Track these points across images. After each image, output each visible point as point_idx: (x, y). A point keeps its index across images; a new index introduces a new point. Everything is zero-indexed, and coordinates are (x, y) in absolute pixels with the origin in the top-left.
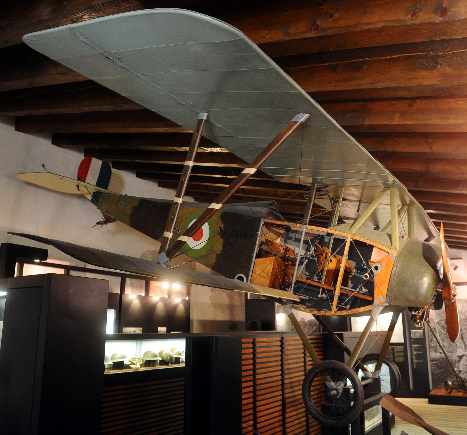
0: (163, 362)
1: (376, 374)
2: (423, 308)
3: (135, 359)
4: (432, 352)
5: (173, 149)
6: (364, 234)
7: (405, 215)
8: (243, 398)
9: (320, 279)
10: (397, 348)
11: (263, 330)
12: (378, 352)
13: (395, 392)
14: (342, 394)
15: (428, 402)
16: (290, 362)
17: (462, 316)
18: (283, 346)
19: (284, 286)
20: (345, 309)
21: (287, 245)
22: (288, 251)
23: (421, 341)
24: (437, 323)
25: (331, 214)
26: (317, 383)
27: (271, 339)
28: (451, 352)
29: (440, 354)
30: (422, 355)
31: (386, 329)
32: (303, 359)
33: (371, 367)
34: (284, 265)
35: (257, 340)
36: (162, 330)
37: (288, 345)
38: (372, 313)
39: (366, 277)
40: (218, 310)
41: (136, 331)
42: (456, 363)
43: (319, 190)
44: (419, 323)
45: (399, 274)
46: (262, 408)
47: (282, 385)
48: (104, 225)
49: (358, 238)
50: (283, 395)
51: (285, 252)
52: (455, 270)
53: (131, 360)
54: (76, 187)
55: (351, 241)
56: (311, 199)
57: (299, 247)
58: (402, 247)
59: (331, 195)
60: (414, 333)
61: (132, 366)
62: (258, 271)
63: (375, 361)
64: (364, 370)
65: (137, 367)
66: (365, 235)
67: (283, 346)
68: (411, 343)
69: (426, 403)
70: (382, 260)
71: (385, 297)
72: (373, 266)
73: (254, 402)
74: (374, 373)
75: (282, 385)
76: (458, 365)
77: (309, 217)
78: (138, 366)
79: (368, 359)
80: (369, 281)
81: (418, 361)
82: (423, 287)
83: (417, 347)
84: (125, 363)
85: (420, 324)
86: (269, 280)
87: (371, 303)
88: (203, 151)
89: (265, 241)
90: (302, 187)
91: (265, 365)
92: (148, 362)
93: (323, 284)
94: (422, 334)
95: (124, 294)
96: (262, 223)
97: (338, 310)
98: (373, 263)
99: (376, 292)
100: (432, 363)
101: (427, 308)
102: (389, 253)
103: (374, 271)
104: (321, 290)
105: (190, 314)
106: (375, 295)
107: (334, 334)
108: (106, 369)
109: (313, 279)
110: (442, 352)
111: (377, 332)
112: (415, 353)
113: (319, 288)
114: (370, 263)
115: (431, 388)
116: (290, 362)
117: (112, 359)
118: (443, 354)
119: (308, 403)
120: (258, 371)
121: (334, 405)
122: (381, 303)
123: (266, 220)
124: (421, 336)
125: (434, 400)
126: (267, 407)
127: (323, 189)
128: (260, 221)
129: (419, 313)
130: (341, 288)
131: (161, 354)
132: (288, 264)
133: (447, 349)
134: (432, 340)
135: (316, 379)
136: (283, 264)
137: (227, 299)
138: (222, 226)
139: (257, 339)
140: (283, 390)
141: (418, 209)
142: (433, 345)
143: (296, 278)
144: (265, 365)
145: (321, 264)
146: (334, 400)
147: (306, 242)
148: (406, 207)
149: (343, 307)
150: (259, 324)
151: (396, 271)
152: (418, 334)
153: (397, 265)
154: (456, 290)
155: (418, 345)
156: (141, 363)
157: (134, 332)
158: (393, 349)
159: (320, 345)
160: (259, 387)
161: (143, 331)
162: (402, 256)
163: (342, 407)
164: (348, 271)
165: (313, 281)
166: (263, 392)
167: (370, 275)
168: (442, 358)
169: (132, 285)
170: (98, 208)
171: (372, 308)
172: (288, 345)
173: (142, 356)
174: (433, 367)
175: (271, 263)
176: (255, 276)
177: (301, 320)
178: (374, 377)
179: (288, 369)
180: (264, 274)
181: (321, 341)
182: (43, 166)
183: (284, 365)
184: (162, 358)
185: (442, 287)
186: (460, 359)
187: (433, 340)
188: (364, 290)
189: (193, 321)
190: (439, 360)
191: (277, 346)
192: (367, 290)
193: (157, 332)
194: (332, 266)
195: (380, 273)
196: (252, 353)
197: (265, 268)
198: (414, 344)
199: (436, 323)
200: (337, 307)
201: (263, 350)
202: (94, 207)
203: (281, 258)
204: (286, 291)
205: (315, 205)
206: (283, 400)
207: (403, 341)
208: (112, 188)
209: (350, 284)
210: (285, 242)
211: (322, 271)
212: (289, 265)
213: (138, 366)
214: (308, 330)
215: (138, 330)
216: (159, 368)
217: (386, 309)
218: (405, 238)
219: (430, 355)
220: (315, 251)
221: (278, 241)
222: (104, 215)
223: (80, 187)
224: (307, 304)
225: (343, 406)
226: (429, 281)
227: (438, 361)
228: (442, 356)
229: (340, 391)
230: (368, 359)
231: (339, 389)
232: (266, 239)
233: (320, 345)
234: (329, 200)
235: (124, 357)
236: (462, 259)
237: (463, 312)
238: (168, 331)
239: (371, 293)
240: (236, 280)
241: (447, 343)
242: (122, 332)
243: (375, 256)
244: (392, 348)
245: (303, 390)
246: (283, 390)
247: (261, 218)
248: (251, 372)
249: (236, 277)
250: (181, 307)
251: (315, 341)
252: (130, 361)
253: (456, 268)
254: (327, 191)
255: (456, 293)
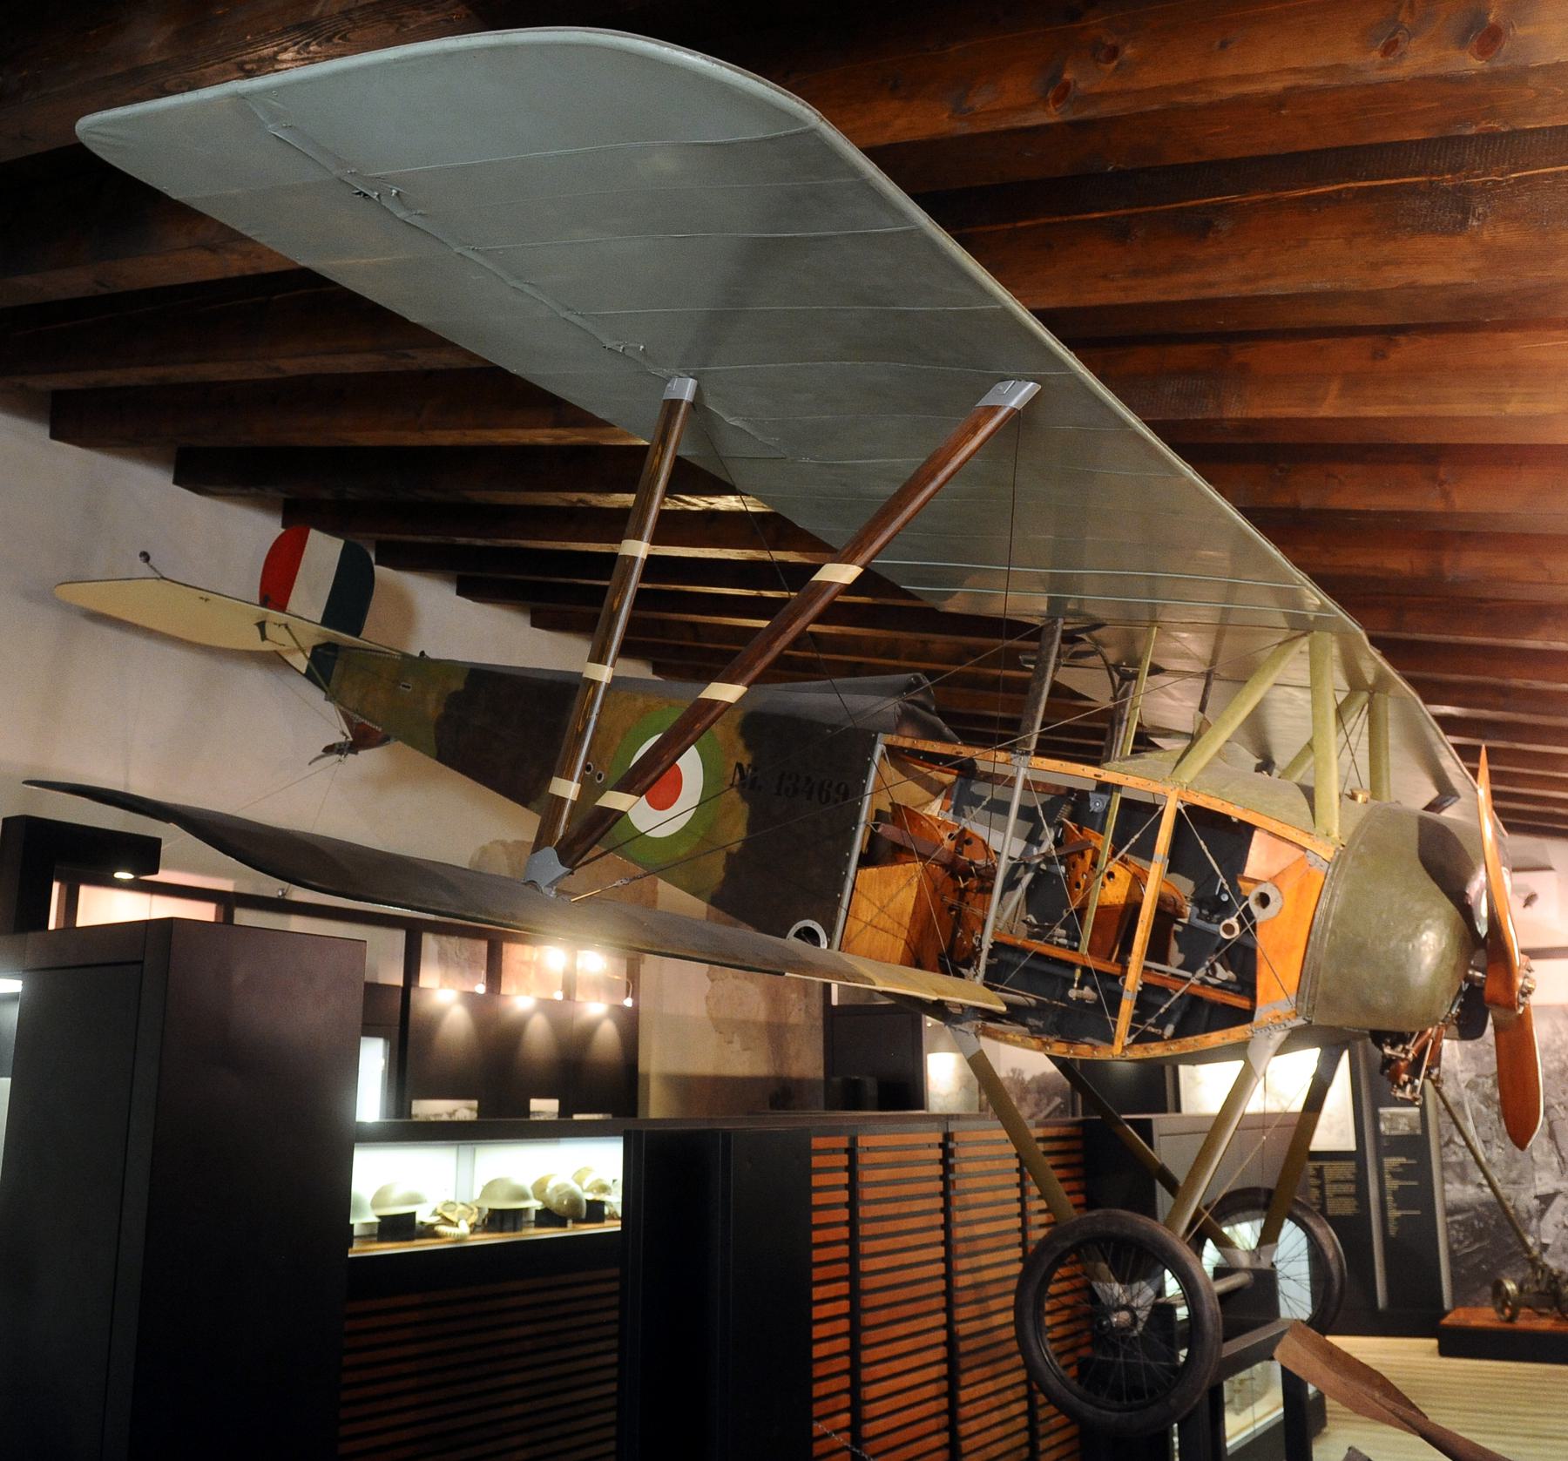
0: (547, 1217)
1: (1262, 1257)
2: (1422, 1033)
3: (452, 1207)
4: (1451, 1183)
5: (580, 501)
6: (1224, 787)
7: (1358, 723)
8: (815, 1336)
9: (1074, 937)
10: (1332, 1170)
11: (882, 1107)
12: (1270, 1182)
13: (1327, 1317)
14: (1148, 1323)
15: (1437, 1350)
16: (974, 1214)
17: (1551, 1062)
18: (951, 1161)
19: (954, 961)
20: (1158, 1038)
21: (964, 823)
22: (968, 842)
23: (1415, 1145)
24: (1467, 1087)
25: (1112, 718)
26: (1064, 1286)
27: (910, 1139)
28: (1514, 1183)
29: (1478, 1190)
30: (1418, 1194)
31: (1297, 1105)
32: (1019, 1205)
33: (1245, 1234)
34: (955, 891)
35: (864, 1141)
36: (545, 1107)
37: (969, 1159)
38: (1251, 1053)
39: (1229, 929)
40: (730, 1042)
41: (455, 1111)
42: (1530, 1218)
43: (1070, 638)
44: (1405, 1084)
45: (1341, 920)
46: (881, 1370)
47: (948, 1293)
48: (351, 756)
49: (1201, 801)
50: (949, 1326)
51: (957, 845)
52: (1528, 908)
53: (439, 1211)
54: (257, 630)
55: (1179, 811)
56: (1045, 670)
57: (1003, 829)
58: (1350, 830)
59: (1112, 655)
60: (1391, 1120)
61: (442, 1229)
62: (866, 911)
63: (1258, 1213)
64: (1223, 1243)
65: (462, 1231)
66: (1226, 790)
67: (951, 1161)
68: (1380, 1154)
69: (1431, 1353)
70: (1282, 873)
71: (1293, 998)
72: (1253, 894)
73: (854, 1352)
74: (1254, 1254)
75: (948, 1293)
76: (1538, 1226)
77: (1037, 729)
78: (464, 1229)
79: (1235, 1204)
80: (1238, 944)
81: (1405, 1213)
82: (1419, 964)
83: (1402, 1165)
84: (419, 1218)
85: (1409, 1087)
86: (903, 942)
87: (1246, 1016)
88: (680, 506)
89: (889, 809)
90: (1014, 628)
91: (889, 1226)
92: (498, 1217)
93: (1083, 955)
94: (1417, 1123)
95: (418, 986)
96: (880, 748)
97: (1135, 1042)
98: (1252, 885)
99: (1262, 980)
100: (1449, 1219)
101: (1434, 1035)
102: (1305, 849)
103: (1256, 909)
104: (1078, 973)
105: (637, 1055)
106: (1260, 992)
107: (1120, 1123)
108: (355, 1240)
109: (1052, 936)
110: (1484, 1182)
111: (1264, 1116)
112: (1392, 1184)
113: (1072, 966)
114: (1241, 883)
115: (1447, 1304)
116: (974, 1214)
117: (374, 1205)
118: (1488, 1190)
119: (1036, 1353)
120: (867, 1247)
121: (1121, 1359)
122: (1278, 1017)
123: (895, 737)
124: (1412, 1128)
125: (1457, 1343)
126: (897, 1366)
127: (1083, 636)
128: (874, 742)
129: (1407, 1052)
130: (1145, 968)
131: (539, 1189)
132: (966, 887)
133: (1501, 1171)
134: (1451, 1141)
135: (1062, 1272)
136: (951, 888)
137: (763, 1005)
138: (746, 760)
139: (864, 1138)
140: (949, 1309)
141: (1402, 700)
142: (1453, 1159)
143: (994, 934)
144: (889, 1226)
145: (1078, 885)
146: (1120, 1344)
147: (1026, 813)
148: (1364, 696)
149: (1153, 1030)
150: (871, 1087)
151: (1329, 909)
152: (1403, 1121)
153: (1334, 889)
154: (1532, 975)
155: (1403, 1160)
156: (474, 1219)
157: (452, 1114)
158: (1319, 1173)
159: (1074, 1159)
160: (869, 1301)
161: (481, 1111)
162: (1350, 858)
163: (1147, 1367)
164: (1169, 909)
165: (1052, 943)
166: (883, 1315)
167: (1242, 925)
168: (1484, 1204)
169: (443, 958)
170: (330, 697)
171: (1250, 1034)
172: (969, 1159)
173: (477, 1195)
174: (1454, 1232)
175: (909, 884)
176: (856, 927)
177: (1011, 1074)
178: (1257, 1266)
179: (966, 1240)
180: (885, 922)
181: (1077, 1145)
182: (145, 556)
183: (952, 1225)
184: (544, 1202)
185: (1483, 964)
186: (1543, 1206)
187: (1454, 1143)
188: (1223, 974)
189: (647, 1077)
190: (1475, 1209)
191: (930, 1162)
192: (1231, 975)
193: (528, 1116)
194: (1114, 892)
195: (1276, 917)
196: (847, 1187)
197: (891, 900)
198: (1390, 1155)
199: (1463, 1085)
200: (1132, 1031)
201: (882, 1174)
202: (316, 695)
203: (943, 866)
204: (961, 976)
205: (1057, 689)
206: (951, 1343)
207: (1352, 1147)
208: (377, 631)
209: (1176, 955)
210: (958, 812)
211: (1081, 911)
212: (971, 891)
213: (464, 1229)
214: (1035, 1110)
215: (462, 1110)
216: (535, 1235)
217: (1295, 1039)
218: (1360, 798)
219: (1444, 1191)
220: (1058, 842)
221: (935, 809)
222: (349, 721)
223: (269, 629)
224: (1031, 1021)
225: (1152, 1364)
226: (1440, 944)
227: (1471, 1214)
228: (1482, 1195)
229: (1142, 1315)
230: (1235, 1204)
231: (1138, 1308)
232: (892, 804)
233: (1074, 1159)
234: (1106, 672)
235: (416, 1200)
236: (1550, 869)
237: (1554, 1047)
238: (565, 1111)
239: (1247, 985)
240: (792, 941)
241: (1499, 1154)
242: (410, 1115)
243: (1259, 860)
244: (1315, 1169)
245: (1018, 1308)
246: (949, 1309)
247: (876, 734)
248: (843, 1251)
249: (794, 930)
250: (608, 1032)
251: (1056, 1146)
252: (435, 1213)
253: (1530, 900)
254: (1097, 642)
255: (1530, 986)
